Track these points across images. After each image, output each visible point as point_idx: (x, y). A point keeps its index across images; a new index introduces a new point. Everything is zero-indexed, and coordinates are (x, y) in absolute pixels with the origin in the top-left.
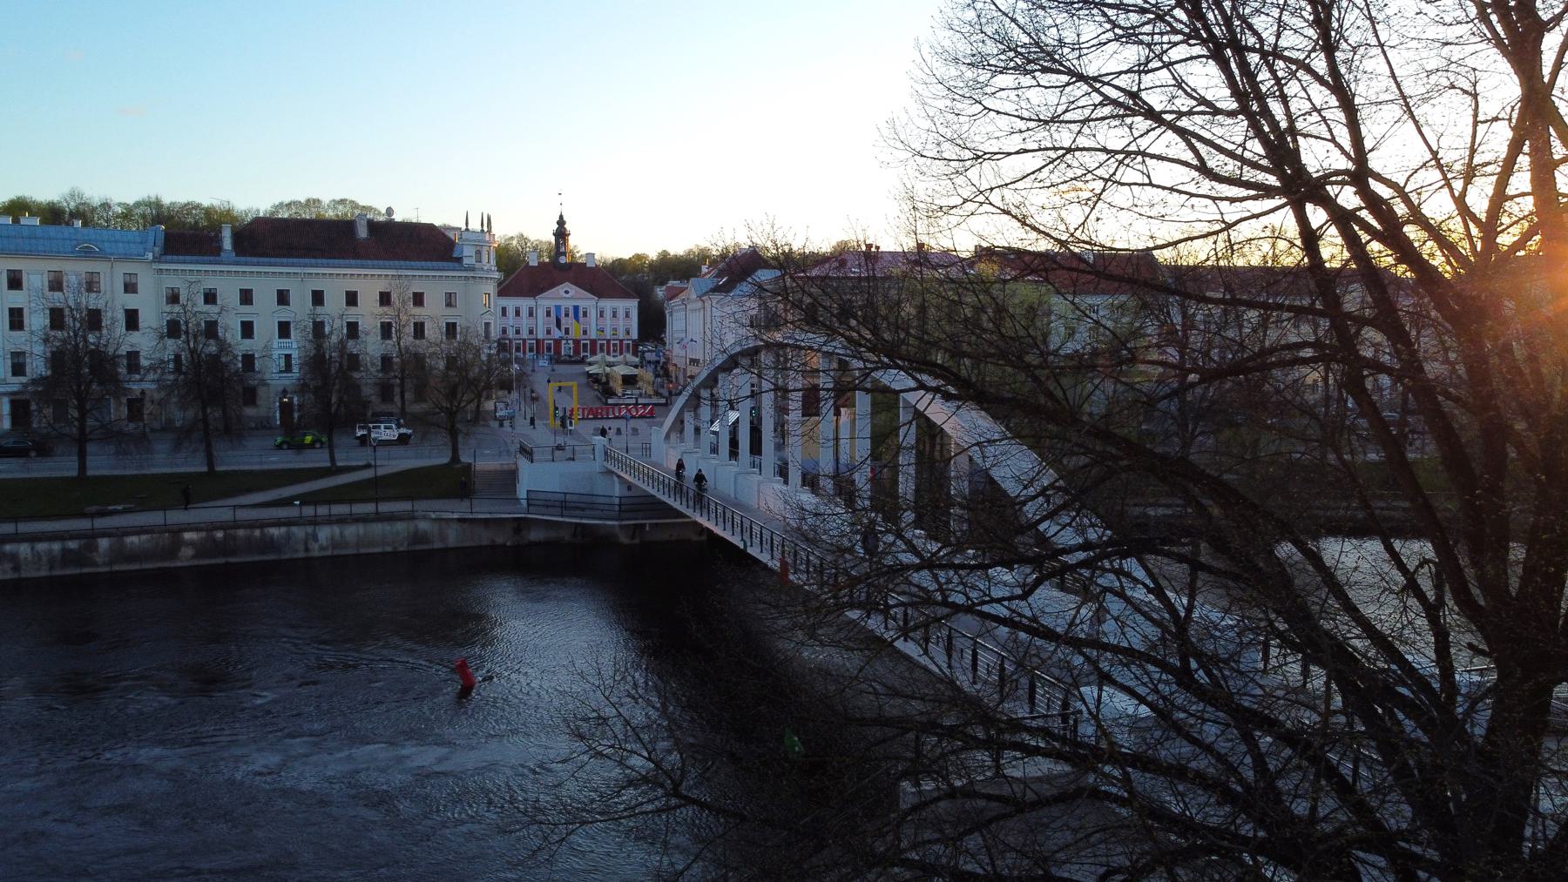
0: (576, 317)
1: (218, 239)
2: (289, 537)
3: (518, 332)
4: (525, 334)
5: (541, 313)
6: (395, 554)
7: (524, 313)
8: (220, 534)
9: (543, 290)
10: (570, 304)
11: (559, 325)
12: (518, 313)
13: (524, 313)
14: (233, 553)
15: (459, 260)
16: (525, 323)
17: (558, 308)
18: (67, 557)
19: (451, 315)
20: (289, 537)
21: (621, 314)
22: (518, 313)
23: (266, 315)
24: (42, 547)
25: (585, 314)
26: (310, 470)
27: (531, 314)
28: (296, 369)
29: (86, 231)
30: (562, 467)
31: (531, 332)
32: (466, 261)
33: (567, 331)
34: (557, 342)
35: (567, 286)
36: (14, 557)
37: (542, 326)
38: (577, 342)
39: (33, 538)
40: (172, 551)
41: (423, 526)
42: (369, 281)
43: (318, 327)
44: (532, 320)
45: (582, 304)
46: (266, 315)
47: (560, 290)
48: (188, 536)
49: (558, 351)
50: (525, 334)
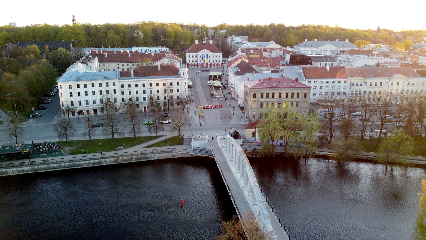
0: (207, 58)
1: (130, 72)
2: (151, 156)
3: (193, 61)
4: (195, 62)
5: (198, 56)
6: (170, 159)
7: (194, 56)
8: (139, 156)
9: (199, 51)
10: (205, 54)
11: (203, 59)
12: (193, 57)
13: (194, 56)
14: (141, 159)
15: (180, 75)
16: (195, 59)
17: (203, 55)
18: (115, 161)
19: (179, 94)
20: (151, 156)
21: (218, 56)
22: (193, 57)
23: (140, 89)
24: (111, 159)
25: (209, 57)
26: (154, 147)
27: (196, 57)
28: (147, 100)
29: (105, 72)
30: (200, 142)
31: (196, 61)
32: (181, 75)
33: (205, 61)
34: (202, 64)
35: (205, 50)
36: (106, 161)
37: (199, 60)
38: (207, 64)
39: (109, 158)
40: (131, 160)
41: (174, 154)
42: (161, 81)
43: (151, 98)
44: (196, 58)
45: (208, 54)
46: (140, 89)
47: (203, 51)
48: (134, 157)
49: (203, 66)
50: (195, 62)
